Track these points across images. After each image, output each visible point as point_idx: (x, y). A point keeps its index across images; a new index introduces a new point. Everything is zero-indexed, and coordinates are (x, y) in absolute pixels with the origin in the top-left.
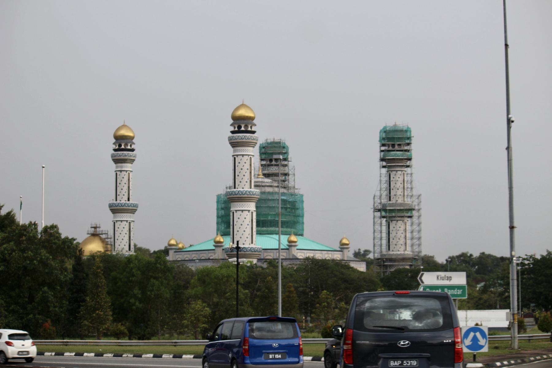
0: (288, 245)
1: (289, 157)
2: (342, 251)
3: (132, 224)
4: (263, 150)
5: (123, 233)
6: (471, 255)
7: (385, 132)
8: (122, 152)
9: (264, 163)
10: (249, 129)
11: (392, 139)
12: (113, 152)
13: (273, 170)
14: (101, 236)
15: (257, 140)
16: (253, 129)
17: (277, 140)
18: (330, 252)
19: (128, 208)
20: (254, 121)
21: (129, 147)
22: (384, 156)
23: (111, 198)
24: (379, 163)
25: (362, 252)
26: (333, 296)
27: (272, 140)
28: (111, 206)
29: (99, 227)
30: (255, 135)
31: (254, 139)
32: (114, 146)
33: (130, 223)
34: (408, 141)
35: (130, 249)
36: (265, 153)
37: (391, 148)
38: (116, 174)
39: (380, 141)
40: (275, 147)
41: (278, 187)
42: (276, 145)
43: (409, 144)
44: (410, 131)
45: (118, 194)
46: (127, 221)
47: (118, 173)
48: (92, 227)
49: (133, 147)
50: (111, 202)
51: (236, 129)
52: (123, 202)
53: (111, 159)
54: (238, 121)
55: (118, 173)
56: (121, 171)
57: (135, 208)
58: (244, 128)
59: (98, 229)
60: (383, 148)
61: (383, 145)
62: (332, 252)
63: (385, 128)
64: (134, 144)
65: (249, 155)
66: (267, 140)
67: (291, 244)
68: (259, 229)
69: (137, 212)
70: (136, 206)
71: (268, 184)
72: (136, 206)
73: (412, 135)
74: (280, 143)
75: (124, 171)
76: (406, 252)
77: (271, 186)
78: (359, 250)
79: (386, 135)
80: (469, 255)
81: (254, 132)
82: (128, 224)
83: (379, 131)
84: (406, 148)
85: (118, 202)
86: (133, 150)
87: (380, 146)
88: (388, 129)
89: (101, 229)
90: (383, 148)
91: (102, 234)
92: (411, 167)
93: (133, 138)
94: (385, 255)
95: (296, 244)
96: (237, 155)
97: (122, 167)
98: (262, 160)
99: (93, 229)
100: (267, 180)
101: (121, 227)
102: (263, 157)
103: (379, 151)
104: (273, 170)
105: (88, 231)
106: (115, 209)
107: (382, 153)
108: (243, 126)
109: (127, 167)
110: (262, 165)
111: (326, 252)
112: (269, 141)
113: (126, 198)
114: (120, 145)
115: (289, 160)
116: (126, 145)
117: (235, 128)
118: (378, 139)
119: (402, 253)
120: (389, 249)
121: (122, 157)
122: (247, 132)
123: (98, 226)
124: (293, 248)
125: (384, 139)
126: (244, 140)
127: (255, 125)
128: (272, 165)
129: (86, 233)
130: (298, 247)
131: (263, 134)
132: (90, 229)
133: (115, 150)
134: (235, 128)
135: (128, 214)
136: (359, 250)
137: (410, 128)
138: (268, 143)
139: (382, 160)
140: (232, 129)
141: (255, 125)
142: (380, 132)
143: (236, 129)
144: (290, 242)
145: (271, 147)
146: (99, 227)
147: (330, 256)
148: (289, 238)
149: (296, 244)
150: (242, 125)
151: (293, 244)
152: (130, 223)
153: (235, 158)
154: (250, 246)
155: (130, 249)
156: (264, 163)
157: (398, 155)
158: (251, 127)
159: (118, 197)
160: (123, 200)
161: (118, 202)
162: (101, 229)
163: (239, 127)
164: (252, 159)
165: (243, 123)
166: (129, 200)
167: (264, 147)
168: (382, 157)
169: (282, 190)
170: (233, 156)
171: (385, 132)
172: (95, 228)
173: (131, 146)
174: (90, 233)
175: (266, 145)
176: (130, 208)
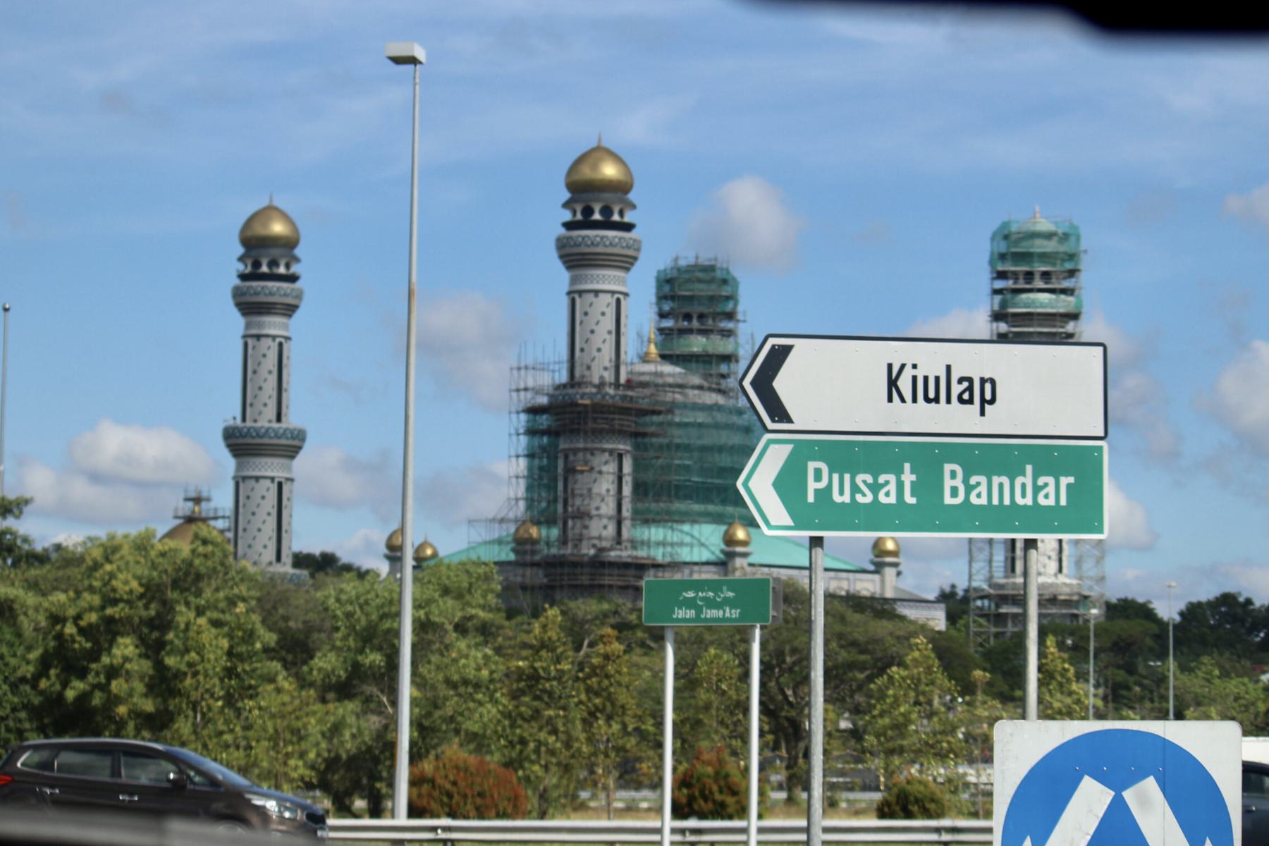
1: (740, 308)
3: (285, 488)
4: (667, 289)
5: (262, 514)
6: (1249, 601)
7: (1006, 237)
8: (262, 283)
9: (668, 323)
10: (616, 217)
11: (1025, 257)
13: (697, 344)
14: (212, 523)
15: (638, 250)
16: (627, 219)
17: (704, 259)
18: (844, 575)
19: (275, 441)
20: (632, 196)
21: (282, 270)
22: (1003, 304)
23: (231, 412)
24: (989, 325)
25: (960, 593)
27: (692, 261)
29: (208, 500)
30: (633, 234)
31: (628, 247)
32: (241, 267)
33: (280, 485)
34: (1068, 266)
35: (279, 558)
36: (673, 298)
37: (1021, 285)
38: (246, 345)
39: (992, 263)
40: (700, 281)
41: (700, 388)
42: (700, 275)
43: (1072, 273)
44: (1078, 238)
45: (248, 401)
46: (272, 479)
47: (251, 342)
48: (187, 499)
49: (295, 269)
51: (579, 217)
52: (263, 423)
53: (230, 303)
54: (584, 196)
55: (251, 342)
56: (258, 337)
57: (296, 443)
59: (204, 505)
60: (1000, 284)
61: (1002, 275)
62: (851, 575)
63: (1005, 225)
64: (297, 260)
65: (613, 292)
66: (676, 259)
68: (640, 505)
70: (300, 436)
71: (670, 380)
72: (300, 436)
73: (1082, 247)
74: (712, 268)
75: (267, 336)
76: (1062, 579)
77: (681, 386)
78: (953, 586)
79: (1008, 247)
80: (1241, 599)
81: (628, 227)
82: (274, 487)
83: (989, 235)
84: (1066, 284)
85: (249, 423)
86: (293, 278)
87: (993, 279)
88: (1014, 228)
89: (212, 505)
90: (1000, 284)
91: (216, 518)
92: (1076, 293)
94: (1002, 587)
96: (581, 293)
97: (260, 325)
98: (662, 315)
99: (190, 504)
100: (668, 368)
102: (666, 307)
103: (988, 291)
104: (697, 344)
105: (176, 509)
106: (242, 444)
107: (998, 298)
108: (597, 208)
109: (273, 325)
110: (661, 331)
112: (682, 263)
113: (271, 412)
114: (257, 264)
115: (740, 317)
116: (273, 263)
118: (986, 257)
119: (1050, 580)
121: (262, 299)
122: (608, 225)
123: (205, 494)
125: (1003, 257)
126: (600, 249)
127: (633, 207)
128: (690, 331)
129: (171, 514)
130: (751, 559)
131: (661, 238)
132: (181, 504)
133: (243, 277)
134: (574, 213)
135: (276, 461)
136: (953, 586)
137: (1076, 228)
138: (679, 270)
139: (997, 317)
140: (567, 216)
141: (633, 207)
142: (993, 239)
143: (579, 217)
145: (689, 281)
146: (208, 500)
147: (845, 585)
148: (726, 533)
150: (594, 212)
151: (739, 549)
152: (280, 485)
155: (279, 558)
156: (668, 323)
157: (1043, 301)
158: (621, 213)
159: (248, 409)
160: (265, 419)
161: (249, 423)
162: (212, 505)
163: (588, 211)
164: (623, 302)
165: (597, 200)
166: (279, 419)
167: (669, 281)
168: (996, 307)
169: (711, 398)
171: (1006, 237)
172: (197, 500)
173: (288, 266)
174: (180, 514)
175: (675, 274)
176: (283, 441)
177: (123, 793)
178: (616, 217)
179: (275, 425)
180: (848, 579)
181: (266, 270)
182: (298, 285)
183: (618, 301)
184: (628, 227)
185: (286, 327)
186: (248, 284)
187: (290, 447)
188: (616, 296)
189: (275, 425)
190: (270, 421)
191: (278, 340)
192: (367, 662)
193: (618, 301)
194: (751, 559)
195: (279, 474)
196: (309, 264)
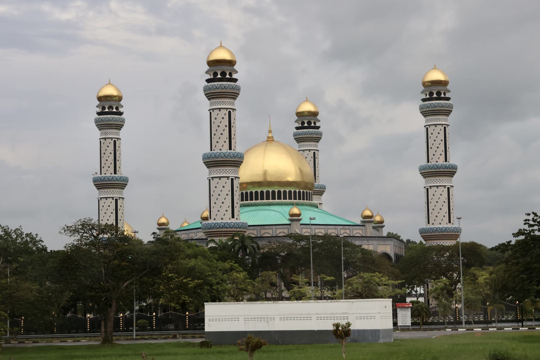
0: (362, 222)
2: (364, 226)
10: (443, 96)
12: (97, 116)
16: (447, 96)
20: (449, 87)
26: (371, 283)
28: (95, 181)
33: (448, 188)
50: (94, 176)
52: (108, 175)
55: (102, 141)
56: (105, 139)
58: (436, 94)
65: (227, 109)
67: (295, 218)
69: (325, 193)
85: (103, 175)
93: (120, 99)
95: (300, 218)
96: (429, 125)
101: (106, 206)
106: (101, 184)
111: (342, 227)
114: (104, 108)
117: (426, 95)
119: (446, 226)
120: (429, 223)
124: (294, 223)
127: (449, 91)
130: (301, 222)
134: (426, 95)
141: (449, 91)
143: (428, 96)
144: (292, 215)
149: (300, 218)
152: (448, 188)
153: (427, 128)
154: (428, 227)
158: (445, 94)
160: (109, 173)
166: (115, 173)
170: (425, 126)
177: (482, 321)
178: (443, 96)
179: (445, 163)
180: (350, 229)
181: (110, 112)
182: (320, 130)
183: (445, 128)
184: (448, 99)
185: (118, 134)
186: (101, 116)
187: (122, 184)
188: (229, 110)
189: (113, 175)
190: (111, 174)
191: (114, 139)
192: (343, 273)
193: (445, 128)
194: (301, 222)
195: (448, 184)
196: (127, 108)
